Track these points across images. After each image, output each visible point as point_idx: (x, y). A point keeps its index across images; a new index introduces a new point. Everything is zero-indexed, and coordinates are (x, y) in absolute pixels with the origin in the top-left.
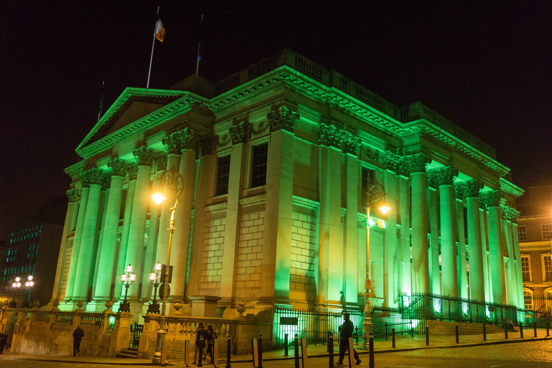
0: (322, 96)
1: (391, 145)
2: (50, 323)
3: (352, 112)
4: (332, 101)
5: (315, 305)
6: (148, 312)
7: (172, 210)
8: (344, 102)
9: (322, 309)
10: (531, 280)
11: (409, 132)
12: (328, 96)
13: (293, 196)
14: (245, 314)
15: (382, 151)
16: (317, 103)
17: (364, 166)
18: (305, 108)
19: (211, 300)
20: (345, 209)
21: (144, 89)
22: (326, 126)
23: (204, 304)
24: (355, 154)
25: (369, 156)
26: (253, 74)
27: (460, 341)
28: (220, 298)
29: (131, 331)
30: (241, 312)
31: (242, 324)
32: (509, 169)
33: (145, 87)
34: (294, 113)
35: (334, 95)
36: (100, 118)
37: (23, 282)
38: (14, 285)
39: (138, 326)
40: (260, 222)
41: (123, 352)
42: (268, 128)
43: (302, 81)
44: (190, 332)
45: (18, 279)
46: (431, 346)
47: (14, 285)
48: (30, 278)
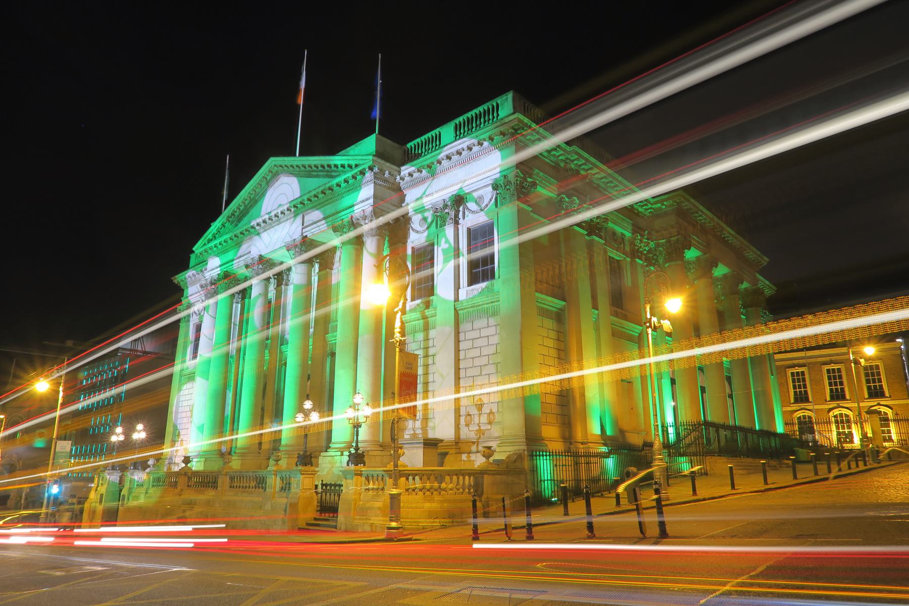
0: (561, 158)
1: (639, 228)
2: (179, 488)
3: (595, 181)
4: (573, 166)
5: (571, 444)
6: (348, 465)
7: (397, 312)
8: (586, 167)
9: (581, 449)
10: (887, 395)
11: (660, 209)
12: (567, 159)
13: (537, 294)
14: (491, 459)
15: (628, 234)
16: (553, 167)
17: (612, 255)
18: (541, 174)
19: (430, 444)
20: (596, 312)
21: (292, 158)
22: (567, 199)
23: (422, 450)
24: (601, 237)
25: (615, 241)
26: (474, 125)
27: (769, 481)
28: (442, 441)
29: (317, 493)
30: (487, 456)
31: (489, 474)
32: (767, 259)
33: (294, 155)
34: (529, 180)
35: (576, 157)
36: (228, 203)
37: (128, 433)
38: (114, 439)
39: (326, 485)
40: (492, 331)
41: (308, 524)
42: (434, 224)
43: (537, 136)
44: (421, 490)
45: (119, 430)
46: (739, 491)
47: (114, 439)
48: (140, 427)
